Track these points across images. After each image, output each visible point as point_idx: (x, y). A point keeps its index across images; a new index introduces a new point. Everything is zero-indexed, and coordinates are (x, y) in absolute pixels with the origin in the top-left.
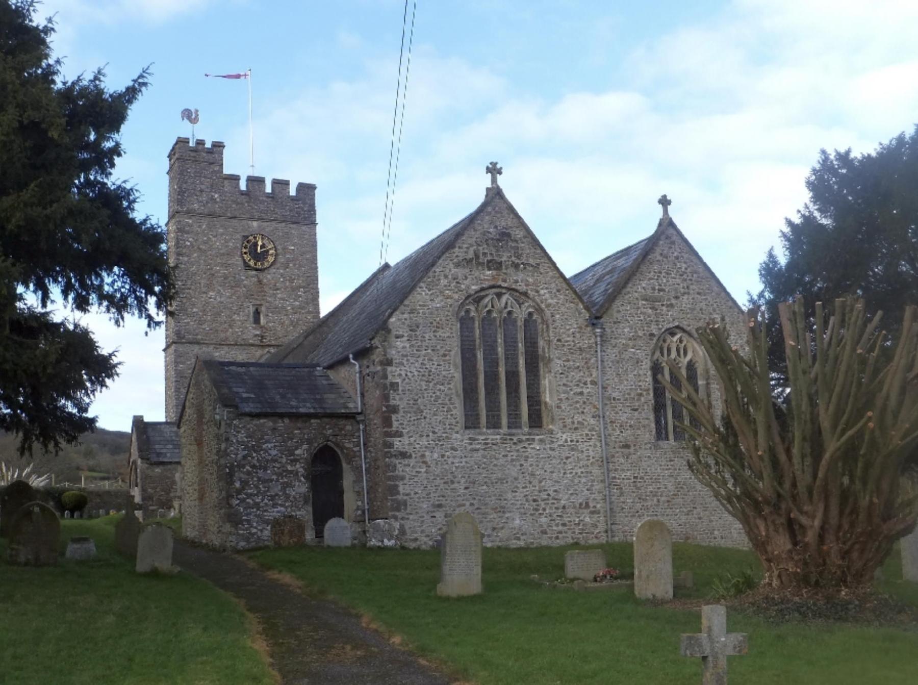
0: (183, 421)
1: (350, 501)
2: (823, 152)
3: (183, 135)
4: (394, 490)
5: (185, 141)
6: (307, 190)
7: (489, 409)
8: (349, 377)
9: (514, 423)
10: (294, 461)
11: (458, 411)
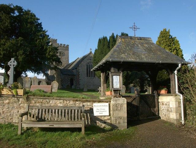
0: (119, 83)
1: (74, 84)
2: (113, 34)
3: (101, 36)
4: (79, 83)
5: (105, 38)
6: (68, 46)
7: (89, 75)
8: (75, 71)
9: (92, 76)
10: (68, 80)
11: (86, 75)
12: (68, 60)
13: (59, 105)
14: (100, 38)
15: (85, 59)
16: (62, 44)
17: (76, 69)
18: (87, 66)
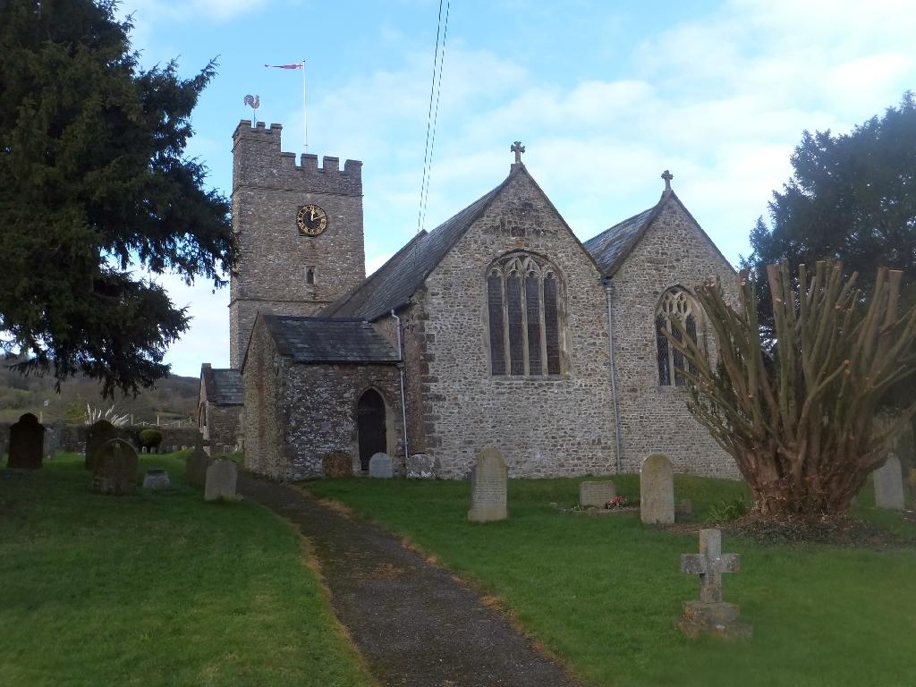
1: (392, 438)
4: (430, 429)
6: (354, 166)
7: (513, 357)
9: (536, 370)
11: (487, 359)
12: (363, 267)
13: (273, 433)
14: (774, 201)
15: (476, 233)
16: (314, 158)
17: (402, 309)
18: (493, 282)
